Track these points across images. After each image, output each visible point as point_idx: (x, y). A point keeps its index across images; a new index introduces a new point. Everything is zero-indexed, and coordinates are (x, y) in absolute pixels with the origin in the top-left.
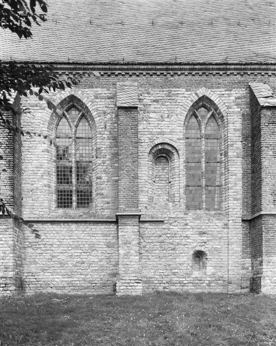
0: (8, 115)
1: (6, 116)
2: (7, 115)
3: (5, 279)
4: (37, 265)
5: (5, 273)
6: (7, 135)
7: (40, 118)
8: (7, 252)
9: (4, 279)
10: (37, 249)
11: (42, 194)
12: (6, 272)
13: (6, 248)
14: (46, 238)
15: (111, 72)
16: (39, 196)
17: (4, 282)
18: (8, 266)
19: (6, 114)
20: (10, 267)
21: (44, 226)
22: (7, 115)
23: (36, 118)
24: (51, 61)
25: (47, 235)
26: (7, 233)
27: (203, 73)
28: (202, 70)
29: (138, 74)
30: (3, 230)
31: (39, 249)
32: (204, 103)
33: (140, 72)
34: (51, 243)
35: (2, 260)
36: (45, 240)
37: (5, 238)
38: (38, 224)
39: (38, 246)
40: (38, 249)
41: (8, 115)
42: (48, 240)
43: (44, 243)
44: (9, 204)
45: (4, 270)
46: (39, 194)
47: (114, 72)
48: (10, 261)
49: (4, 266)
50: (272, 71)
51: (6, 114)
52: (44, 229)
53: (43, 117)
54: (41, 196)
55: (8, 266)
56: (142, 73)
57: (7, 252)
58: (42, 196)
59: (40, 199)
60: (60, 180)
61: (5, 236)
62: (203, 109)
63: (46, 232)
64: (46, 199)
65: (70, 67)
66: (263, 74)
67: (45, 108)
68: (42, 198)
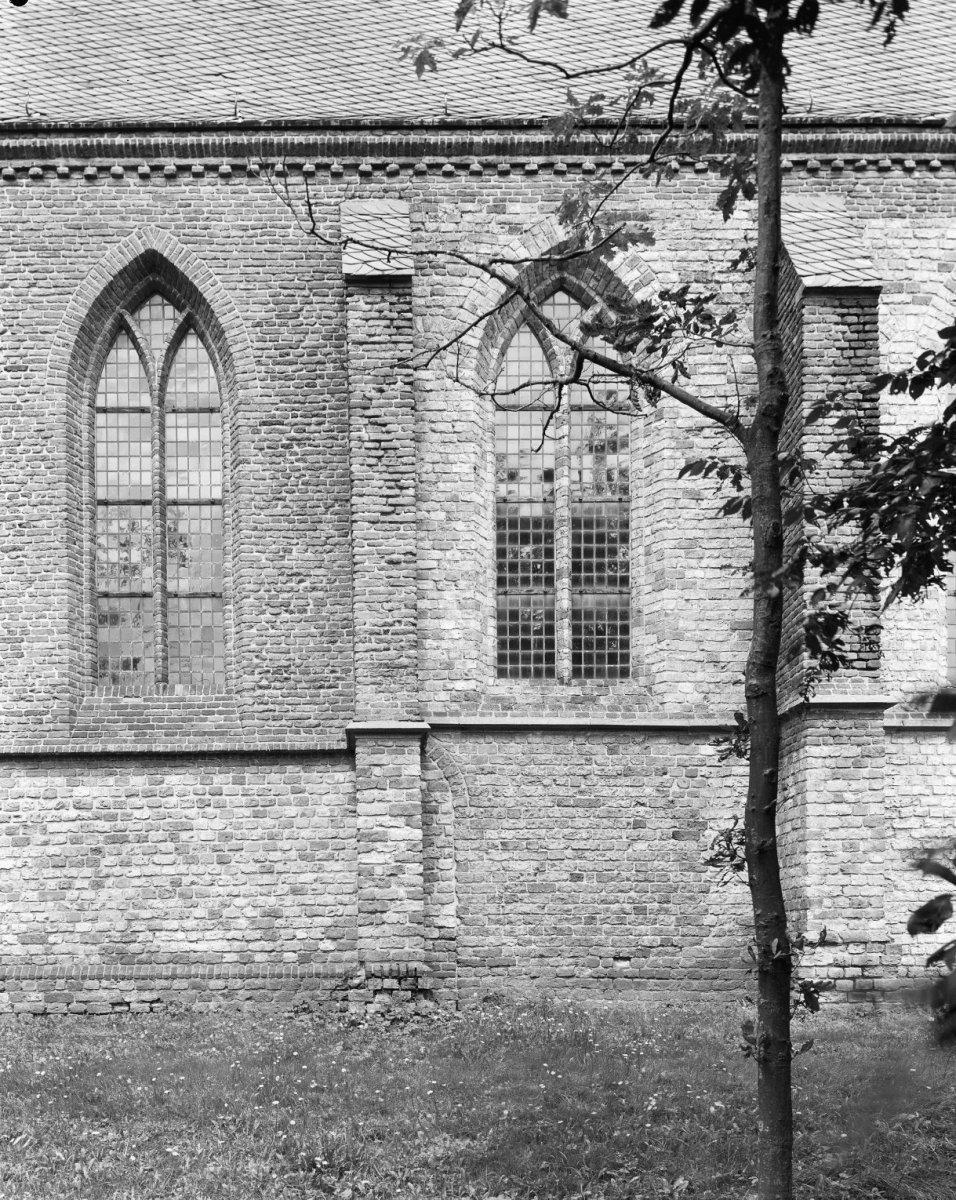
0: (865, 324)
1: (853, 328)
2: (858, 323)
3: (862, 946)
4: (895, 892)
5: (853, 923)
6: (858, 401)
7: (911, 338)
8: (863, 846)
9: (860, 949)
10: (894, 836)
11: (915, 625)
12: (856, 921)
13: (856, 831)
14: (927, 792)
15: (819, 156)
16: (905, 632)
17: (857, 960)
18: (866, 900)
19: (854, 319)
20: (872, 900)
21: (923, 748)
22: (858, 323)
23: (898, 337)
24: (166, 119)
25: (931, 780)
26: (864, 772)
27: (919, 163)
28: (343, 154)
29: (309, 167)
30: (849, 762)
31: (903, 832)
32: (566, 275)
33: (320, 160)
34: (947, 813)
35: (840, 876)
36: (924, 800)
37: (856, 792)
38: (900, 741)
39: (897, 824)
40: (898, 832)
41: (865, 324)
42: (933, 800)
43: (919, 811)
44: (863, 664)
45: (849, 912)
46: (904, 624)
47: (299, 160)
48: (871, 880)
49: (849, 898)
50: (943, 151)
51: (854, 319)
52: (921, 759)
53: (923, 332)
54: (912, 632)
55: (866, 900)
56: (327, 167)
57: (863, 846)
58: (915, 635)
59: (908, 645)
60: (598, 556)
61: (855, 785)
62: (561, 297)
63: (930, 770)
64: (930, 644)
65: (889, 137)
66: (910, 163)
67: (930, 299)
68: (914, 641)
